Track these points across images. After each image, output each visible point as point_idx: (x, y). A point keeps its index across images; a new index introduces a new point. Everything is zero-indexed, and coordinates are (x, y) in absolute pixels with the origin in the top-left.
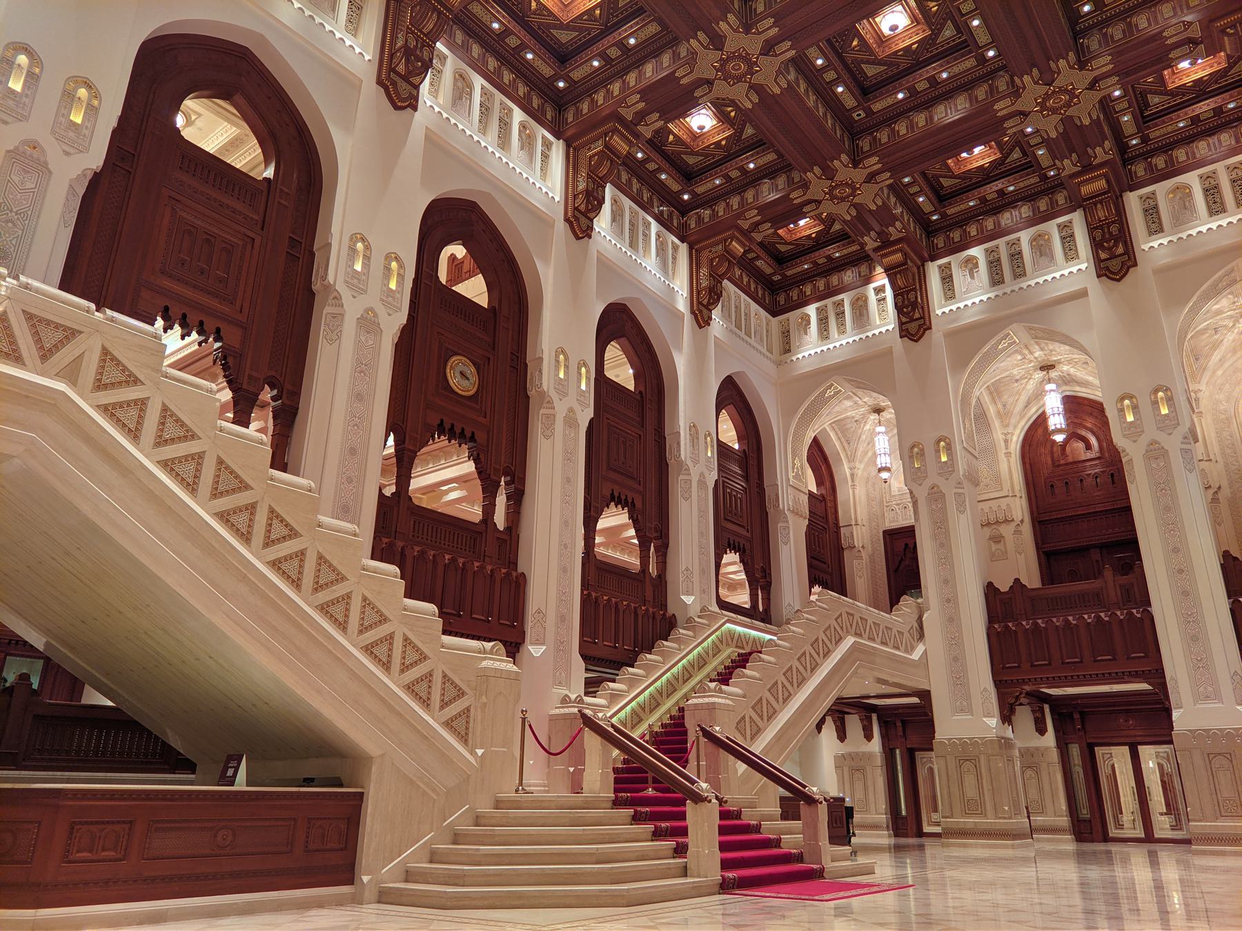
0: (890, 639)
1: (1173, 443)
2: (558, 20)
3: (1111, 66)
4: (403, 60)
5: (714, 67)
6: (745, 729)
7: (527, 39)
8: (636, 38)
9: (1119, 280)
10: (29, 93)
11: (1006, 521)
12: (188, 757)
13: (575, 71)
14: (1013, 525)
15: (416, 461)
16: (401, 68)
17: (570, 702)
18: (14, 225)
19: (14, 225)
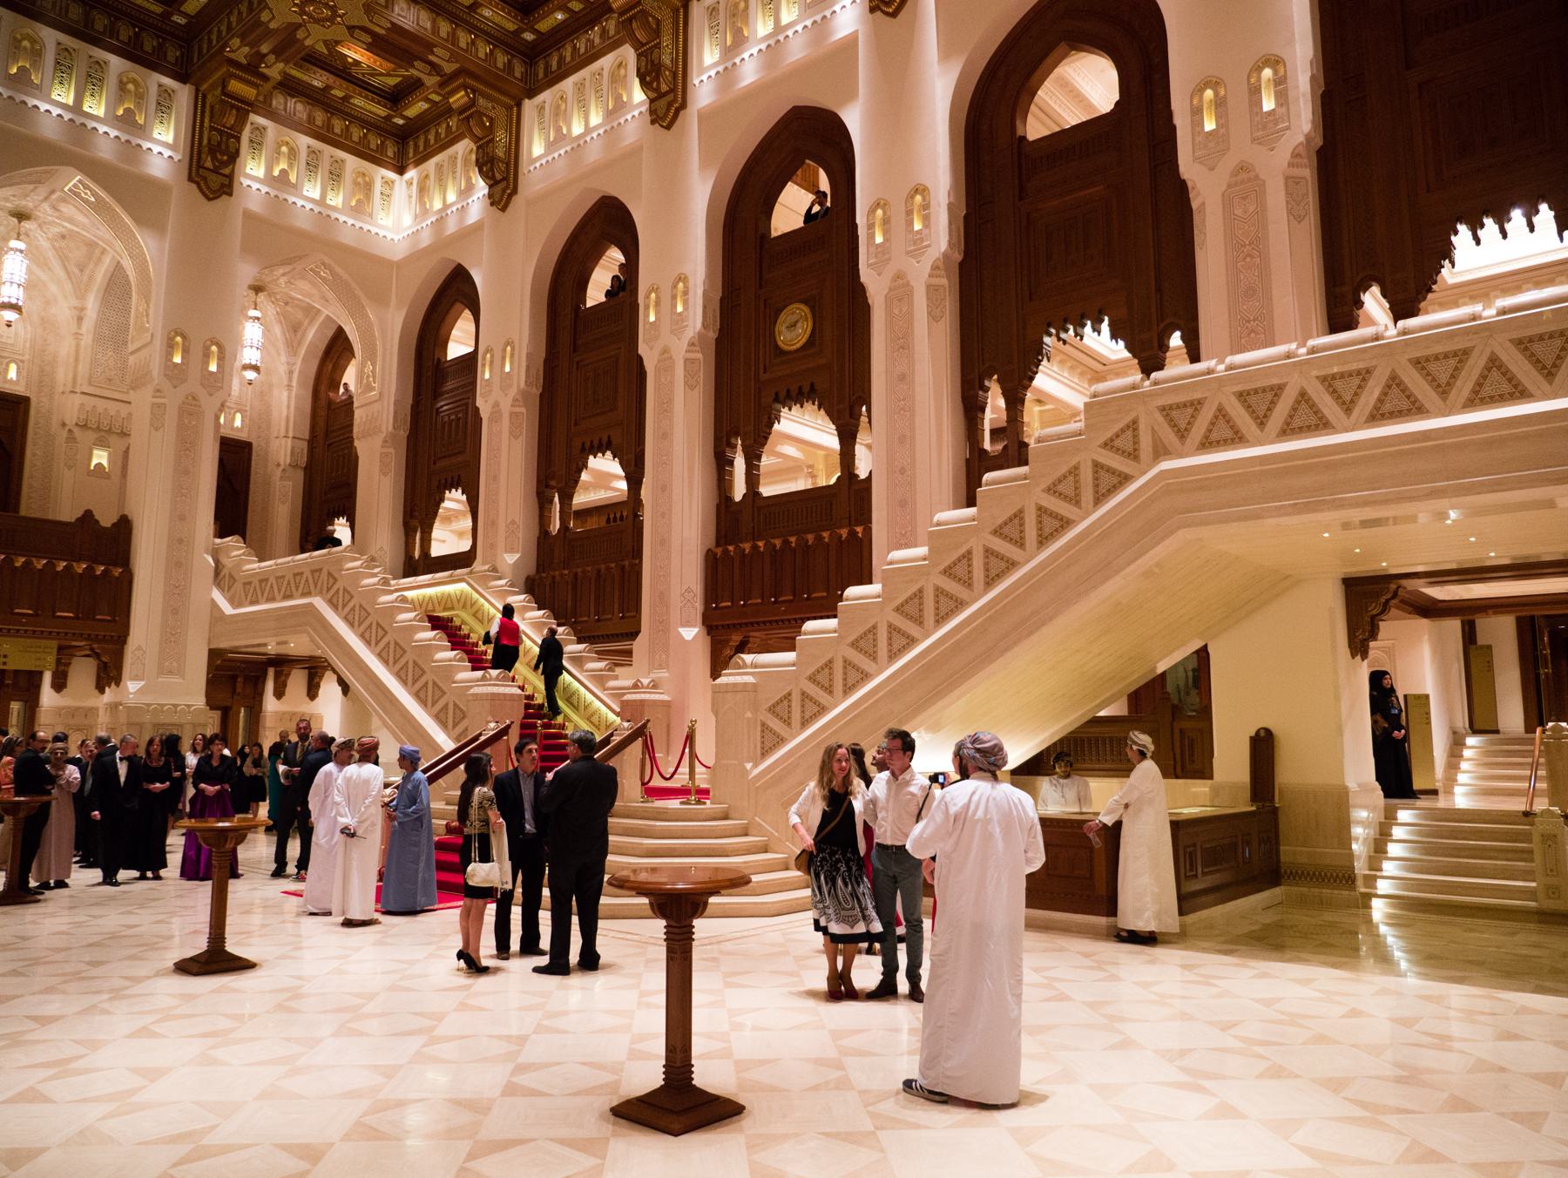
1: (209, 404)
6: (454, 714)
9: (209, 199)
12: (936, 883)
15: (51, 517)
16: (209, 164)
17: (643, 687)
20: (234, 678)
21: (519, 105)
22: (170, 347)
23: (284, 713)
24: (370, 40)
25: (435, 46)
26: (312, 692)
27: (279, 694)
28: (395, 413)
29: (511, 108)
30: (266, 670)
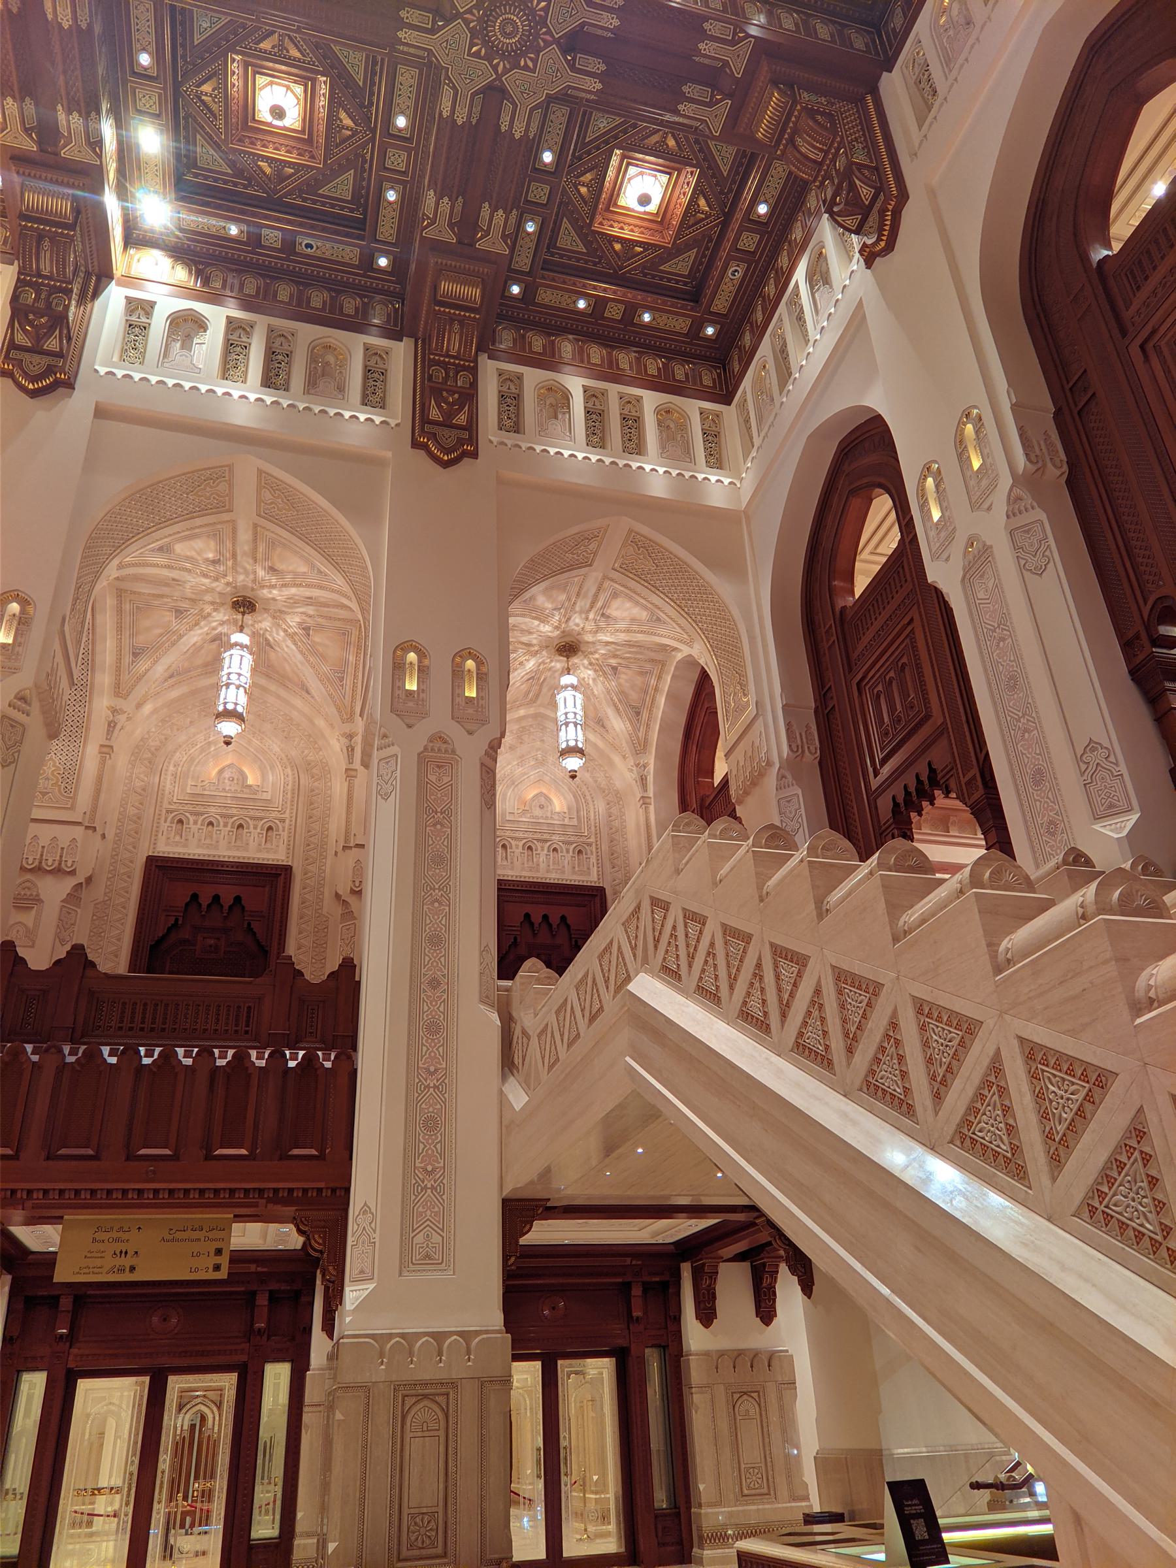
0: (691, 958)
2: (661, 247)
3: (503, 129)
4: (433, 402)
5: (477, 54)
7: (631, 295)
8: (766, 201)
10: (483, 694)
11: (58, 871)
13: (716, 302)
14: (70, 883)
18: (442, 825)
19: (442, 825)
20: (625, 1289)
21: (874, 91)
22: (398, 668)
23: (722, 1354)
24: (603, 67)
25: (706, 19)
26: (766, 1311)
27: (707, 1315)
28: (789, 726)
29: (863, 100)
30: (679, 1269)
